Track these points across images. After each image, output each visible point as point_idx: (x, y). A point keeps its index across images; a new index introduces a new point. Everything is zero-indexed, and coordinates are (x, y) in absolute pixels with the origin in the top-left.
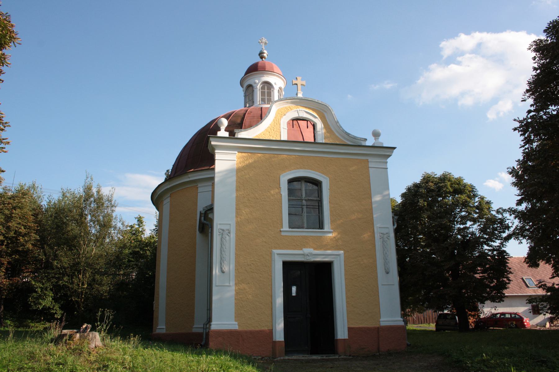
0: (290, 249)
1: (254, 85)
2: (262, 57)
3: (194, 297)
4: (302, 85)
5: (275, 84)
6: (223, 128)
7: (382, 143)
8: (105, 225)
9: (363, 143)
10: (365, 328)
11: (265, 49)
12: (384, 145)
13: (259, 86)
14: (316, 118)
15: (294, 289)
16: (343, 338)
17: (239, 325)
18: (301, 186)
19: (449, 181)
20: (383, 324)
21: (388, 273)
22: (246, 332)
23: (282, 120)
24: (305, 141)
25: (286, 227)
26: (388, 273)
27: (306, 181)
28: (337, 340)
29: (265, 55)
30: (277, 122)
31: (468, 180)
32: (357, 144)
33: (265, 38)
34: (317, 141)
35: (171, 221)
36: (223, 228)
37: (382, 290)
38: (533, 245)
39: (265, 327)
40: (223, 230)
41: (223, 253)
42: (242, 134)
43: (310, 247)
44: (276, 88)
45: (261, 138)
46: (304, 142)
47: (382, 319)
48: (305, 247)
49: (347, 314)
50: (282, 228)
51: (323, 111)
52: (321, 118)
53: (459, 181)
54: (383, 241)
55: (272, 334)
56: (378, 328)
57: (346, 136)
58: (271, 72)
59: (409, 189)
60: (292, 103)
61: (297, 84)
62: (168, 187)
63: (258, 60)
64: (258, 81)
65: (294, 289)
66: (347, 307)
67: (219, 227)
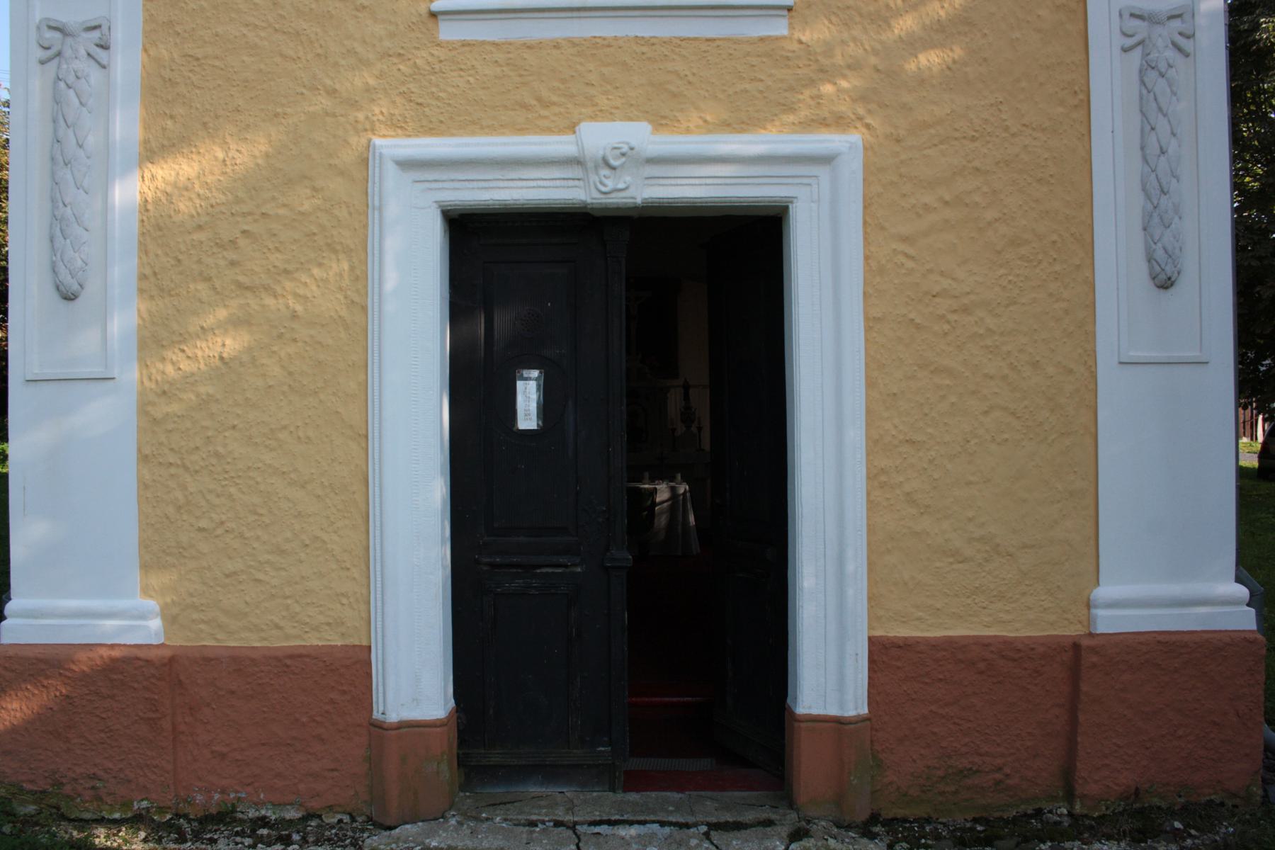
0: (492, 129)
10: (983, 643)
16: (833, 711)
17: (170, 620)
20: (1108, 622)
21: (1166, 284)
26: (1166, 284)
38: (647, 475)
39: (318, 633)
43: (629, 112)
47: (1104, 592)
54: (1148, 66)
56: (1076, 647)
66: (872, 505)
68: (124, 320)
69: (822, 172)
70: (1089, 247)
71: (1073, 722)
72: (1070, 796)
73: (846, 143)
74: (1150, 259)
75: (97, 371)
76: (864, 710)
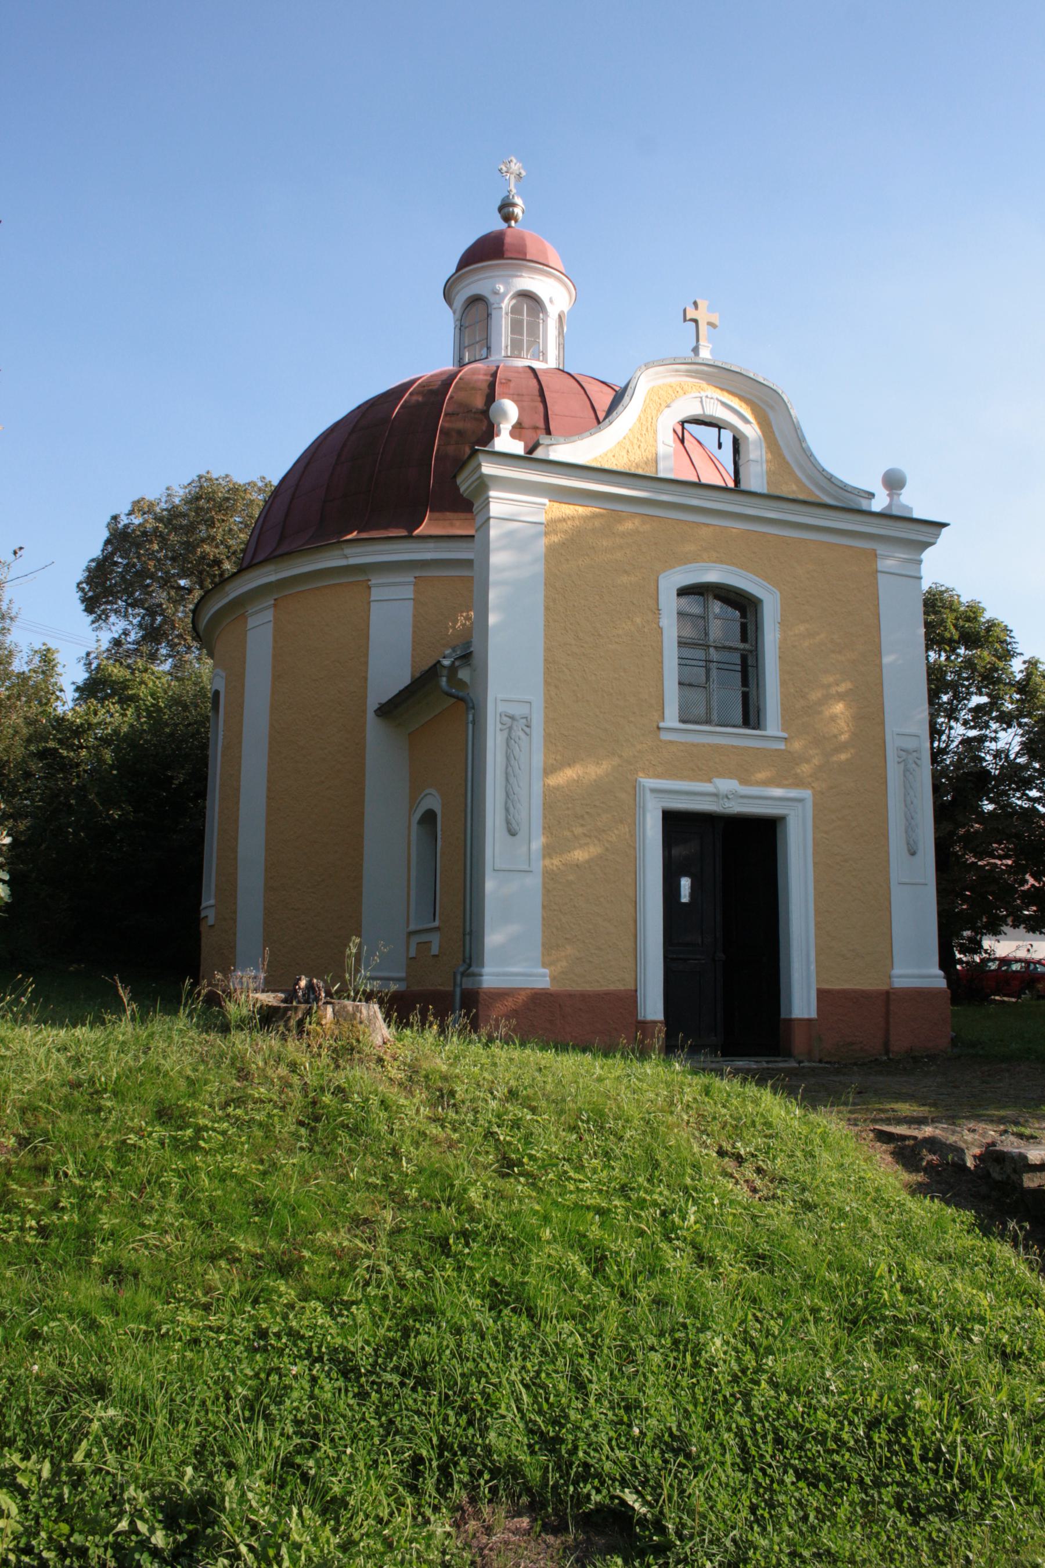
0: (682, 778)
1: (492, 299)
2: (508, 218)
3: (360, 894)
4: (709, 324)
5: (551, 301)
6: (505, 428)
7: (911, 509)
9: (864, 505)
10: (855, 991)
11: (518, 194)
12: (916, 515)
13: (507, 304)
14: (746, 421)
15: (685, 883)
16: (806, 1016)
17: (553, 979)
18: (706, 607)
19: (953, 610)
20: (898, 983)
22: (571, 996)
23: (661, 419)
24: (704, 481)
25: (671, 718)
27: (717, 597)
28: (790, 1020)
29: (517, 211)
30: (647, 424)
31: (994, 610)
32: (847, 504)
33: (519, 161)
34: (743, 486)
35: (277, 677)
36: (511, 712)
37: (899, 897)
40: (512, 718)
41: (512, 780)
42: (561, 451)
44: (553, 311)
45: (606, 466)
46: (699, 485)
47: (896, 971)
48: (721, 775)
49: (817, 955)
50: (663, 719)
51: (765, 402)
52: (759, 423)
53: (973, 613)
55: (636, 1002)
57: (824, 483)
58: (541, 265)
59: (88, 569)
60: (689, 374)
61: (696, 321)
62: (273, 578)
63: (499, 225)
64: (504, 287)
65: (685, 883)
67: (502, 708)
68: (538, 843)
69: (800, 805)
70: (887, 839)
71: (887, 1023)
72: (887, 1052)
73: (807, 794)
74: (908, 844)
75: (525, 867)
76: (813, 1014)
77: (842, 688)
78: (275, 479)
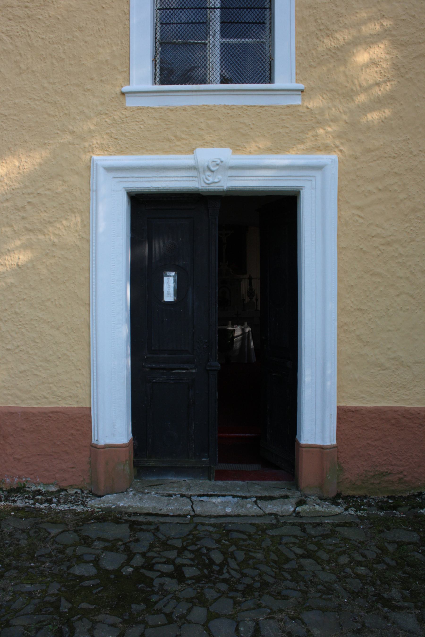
0: (152, 152)
8: (229, 588)
16: (319, 443)
39: (64, 400)
50: (128, 81)
66: (340, 341)
69: (318, 174)
73: (329, 159)
76: (334, 442)
77: (374, 28)
78: (132, 437)
